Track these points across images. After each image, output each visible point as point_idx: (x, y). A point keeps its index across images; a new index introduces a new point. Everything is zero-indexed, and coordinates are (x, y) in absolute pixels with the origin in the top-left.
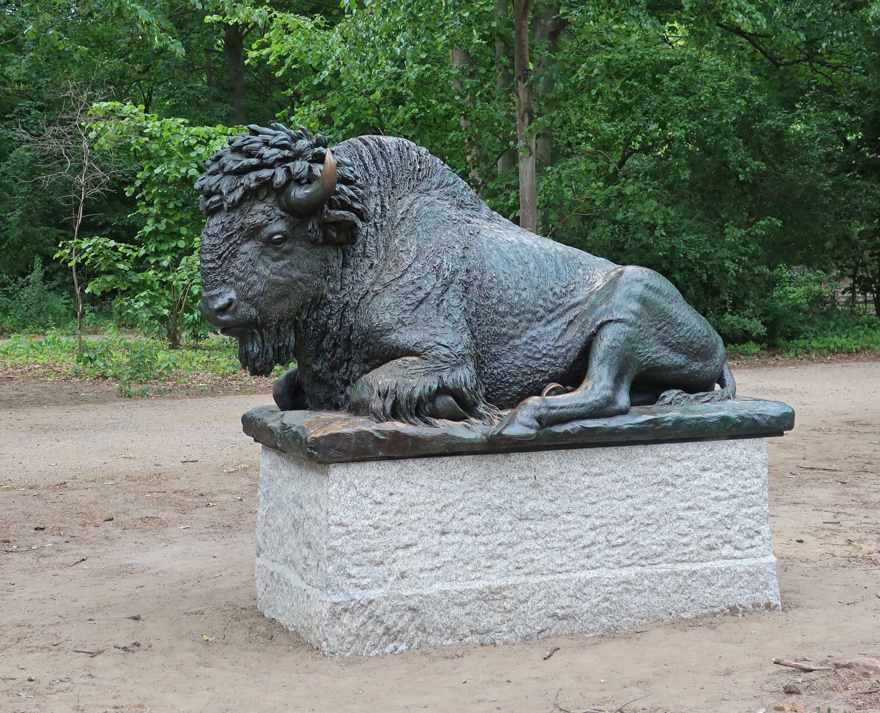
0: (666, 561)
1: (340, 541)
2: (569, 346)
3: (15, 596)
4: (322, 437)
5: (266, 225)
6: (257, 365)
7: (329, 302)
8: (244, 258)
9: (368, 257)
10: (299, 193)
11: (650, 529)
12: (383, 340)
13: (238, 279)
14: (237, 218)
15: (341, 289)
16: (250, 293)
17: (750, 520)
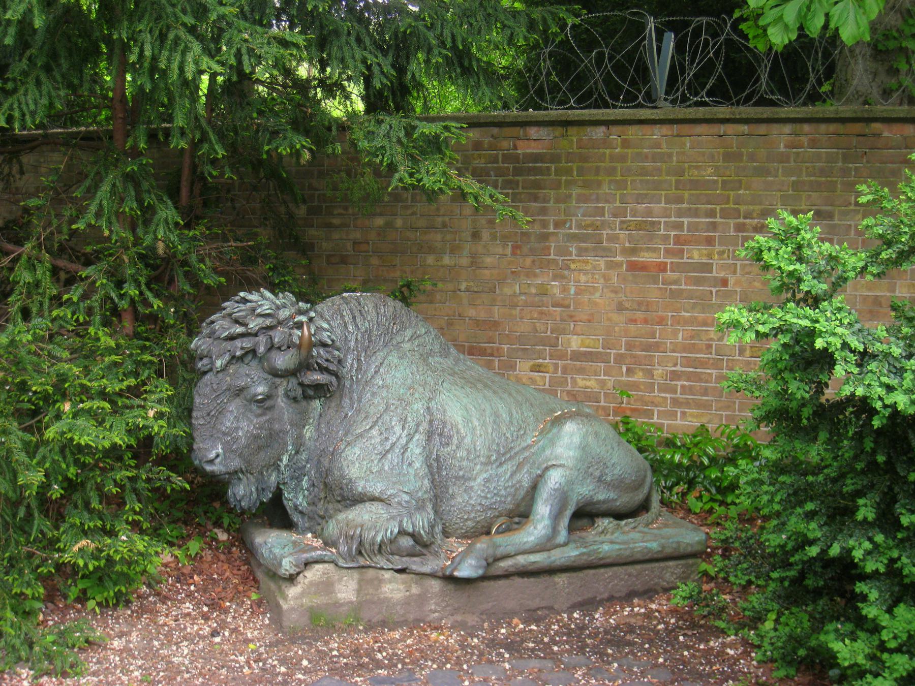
3: (413, 319)
16: (235, 447)
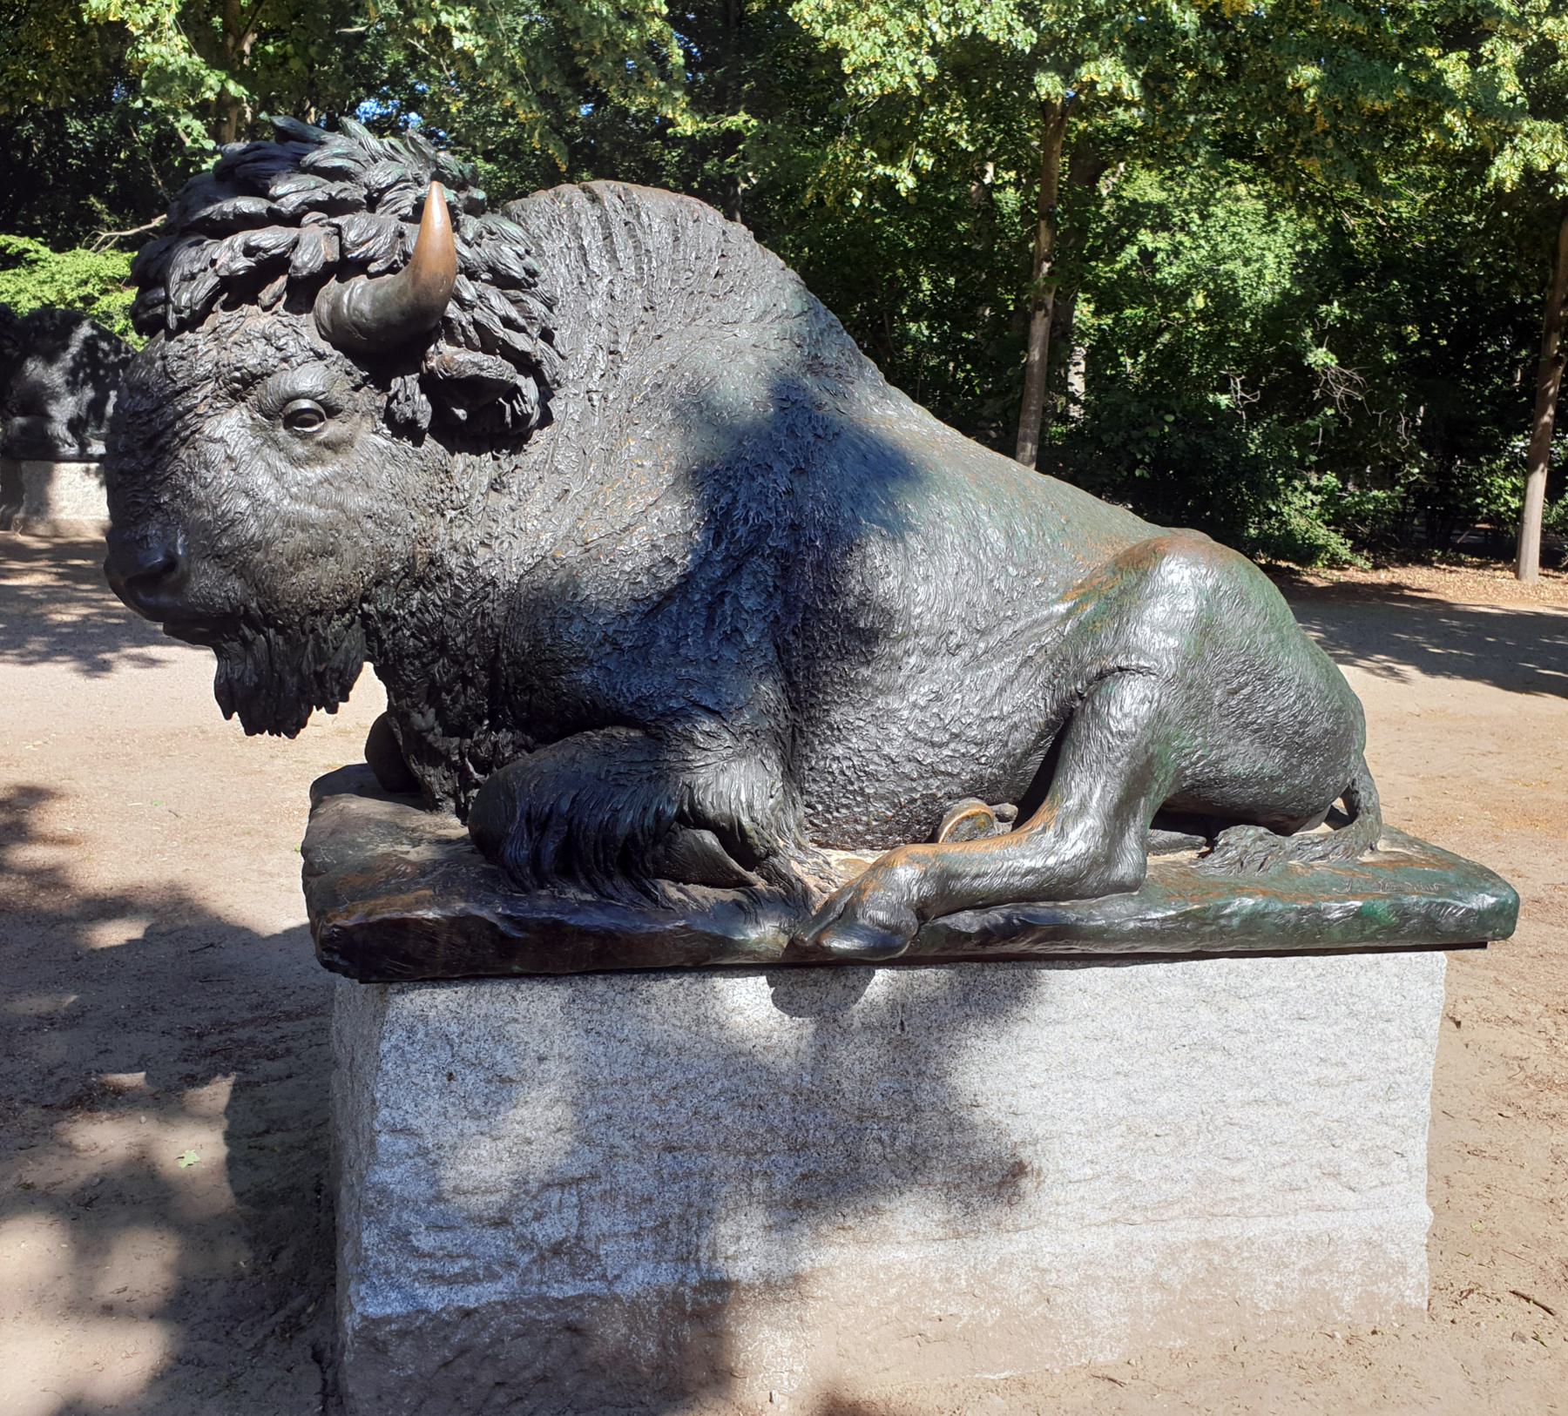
0: (1190, 1215)
1: (399, 1170)
2: (1016, 718)
11: (1159, 1145)
17: (1385, 1129)
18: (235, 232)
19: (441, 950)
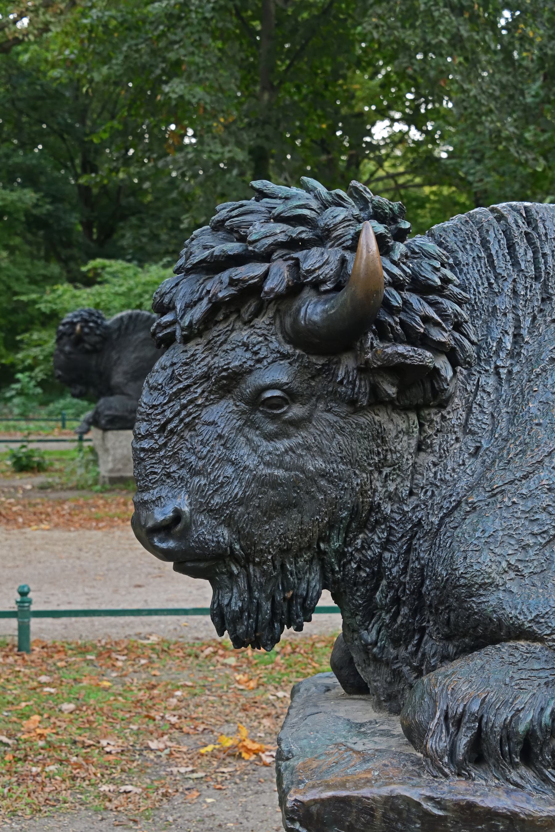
4: (315, 801)
5: (250, 372)
6: (241, 630)
7: (386, 519)
8: (207, 432)
9: (473, 433)
10: (313, 310)
12: (473, 604)
13: (195, 472)
14: (199, 357)
15: (411, 493)
18: (224, 269)
19: (377, 822)
